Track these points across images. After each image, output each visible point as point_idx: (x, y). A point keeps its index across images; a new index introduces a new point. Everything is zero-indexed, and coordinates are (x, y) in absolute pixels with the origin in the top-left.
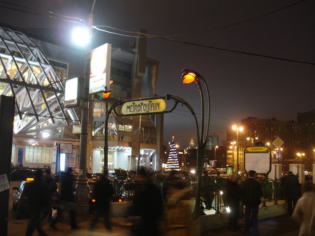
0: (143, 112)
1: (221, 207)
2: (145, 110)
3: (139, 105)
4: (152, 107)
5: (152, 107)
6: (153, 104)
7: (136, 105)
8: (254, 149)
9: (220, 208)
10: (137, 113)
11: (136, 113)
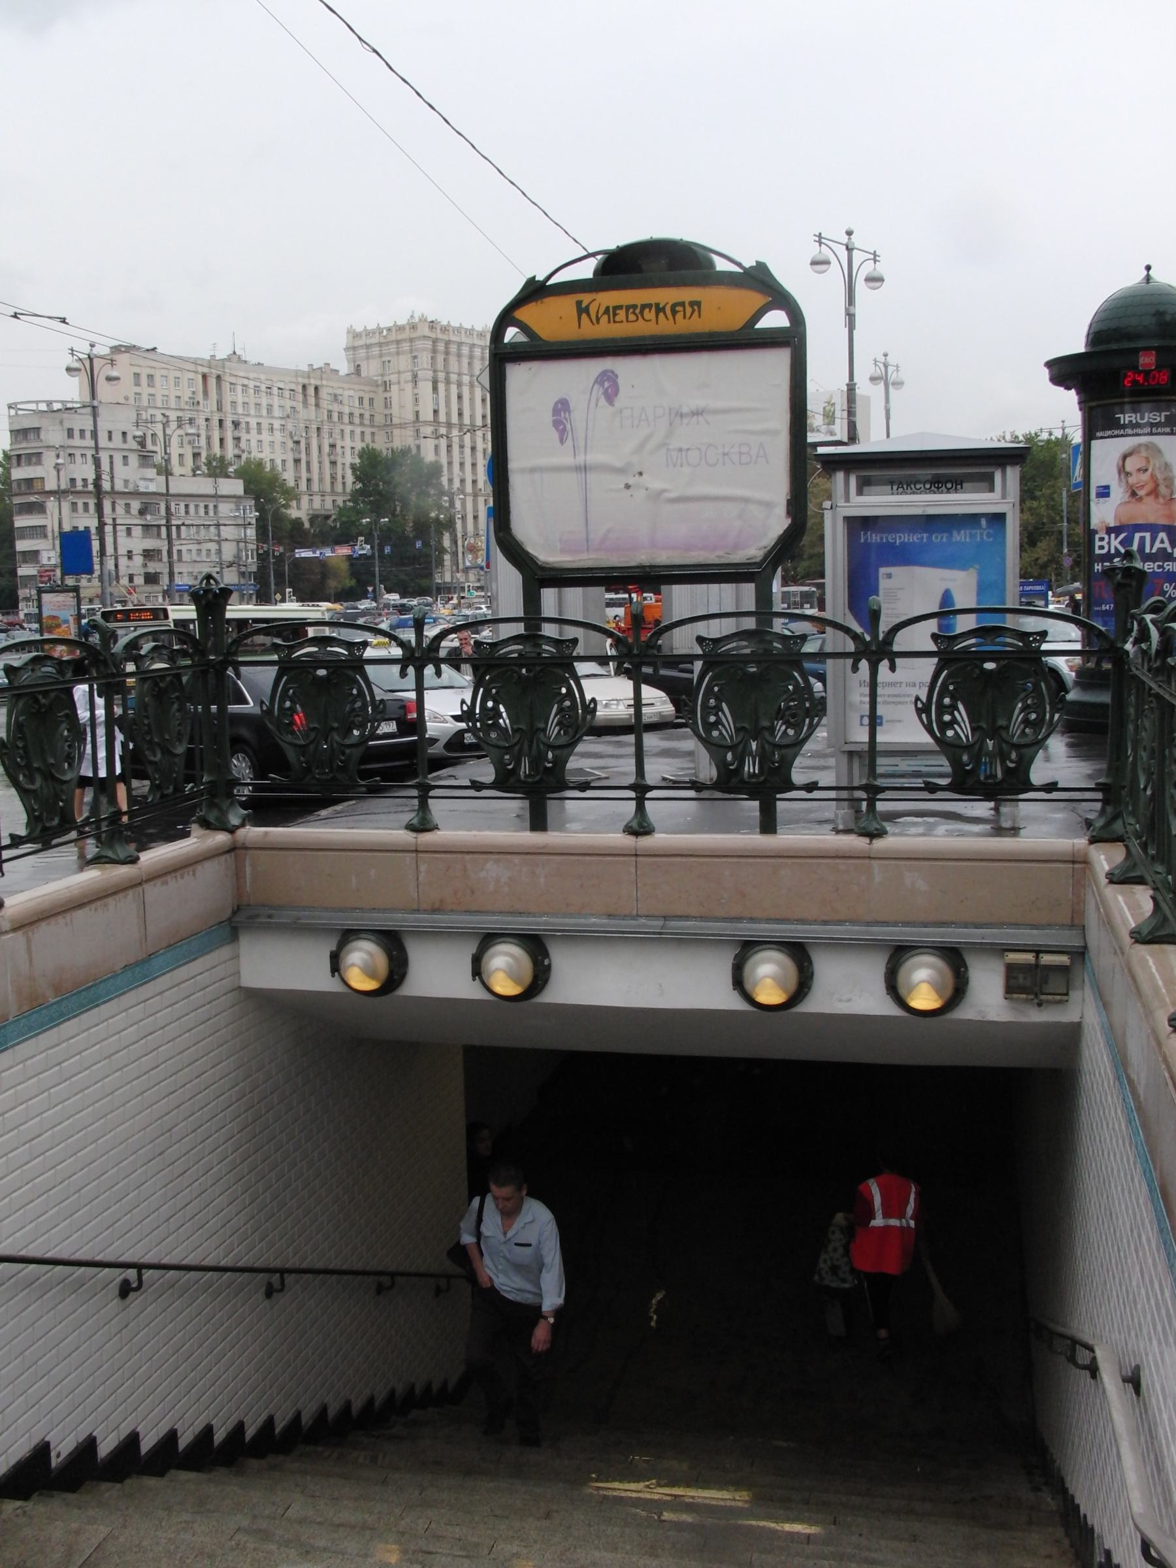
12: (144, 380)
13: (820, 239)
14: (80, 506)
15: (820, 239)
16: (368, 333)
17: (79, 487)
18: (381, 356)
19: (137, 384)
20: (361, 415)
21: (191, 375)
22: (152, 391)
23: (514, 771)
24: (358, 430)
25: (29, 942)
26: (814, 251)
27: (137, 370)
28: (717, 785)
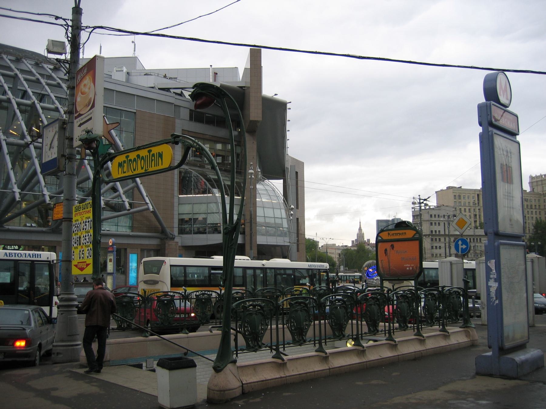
0: (140, 171)
1: (393, 330)
2: (142, 168)
3: (135, 160)
4: (152, 160)
5: (152, 160)
6: (153, 155)
7: (130, 160)
8: (393, 234)
9: (360, 336)
10: (132, 174)
11: (130, 173)
12: (457, 197)
13: (414, 198)
14: (434, 239)
15: (414, 198)
16: (537, 177)
17: (437, 233)
18: (542, 184)
19: (455, 199)
20: (535, 206)
21: (473, 195)
22: (460, 201)
23: (121, 326)
24: (534, 211)
25: (212, 361)
26: (413, 200)
27: (455, 194)
28: (117, 329)
